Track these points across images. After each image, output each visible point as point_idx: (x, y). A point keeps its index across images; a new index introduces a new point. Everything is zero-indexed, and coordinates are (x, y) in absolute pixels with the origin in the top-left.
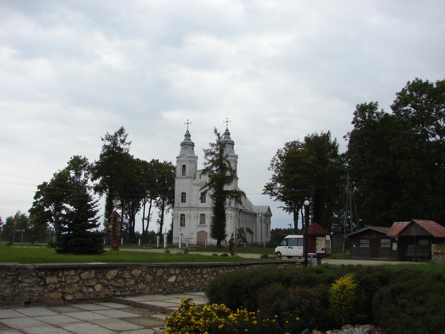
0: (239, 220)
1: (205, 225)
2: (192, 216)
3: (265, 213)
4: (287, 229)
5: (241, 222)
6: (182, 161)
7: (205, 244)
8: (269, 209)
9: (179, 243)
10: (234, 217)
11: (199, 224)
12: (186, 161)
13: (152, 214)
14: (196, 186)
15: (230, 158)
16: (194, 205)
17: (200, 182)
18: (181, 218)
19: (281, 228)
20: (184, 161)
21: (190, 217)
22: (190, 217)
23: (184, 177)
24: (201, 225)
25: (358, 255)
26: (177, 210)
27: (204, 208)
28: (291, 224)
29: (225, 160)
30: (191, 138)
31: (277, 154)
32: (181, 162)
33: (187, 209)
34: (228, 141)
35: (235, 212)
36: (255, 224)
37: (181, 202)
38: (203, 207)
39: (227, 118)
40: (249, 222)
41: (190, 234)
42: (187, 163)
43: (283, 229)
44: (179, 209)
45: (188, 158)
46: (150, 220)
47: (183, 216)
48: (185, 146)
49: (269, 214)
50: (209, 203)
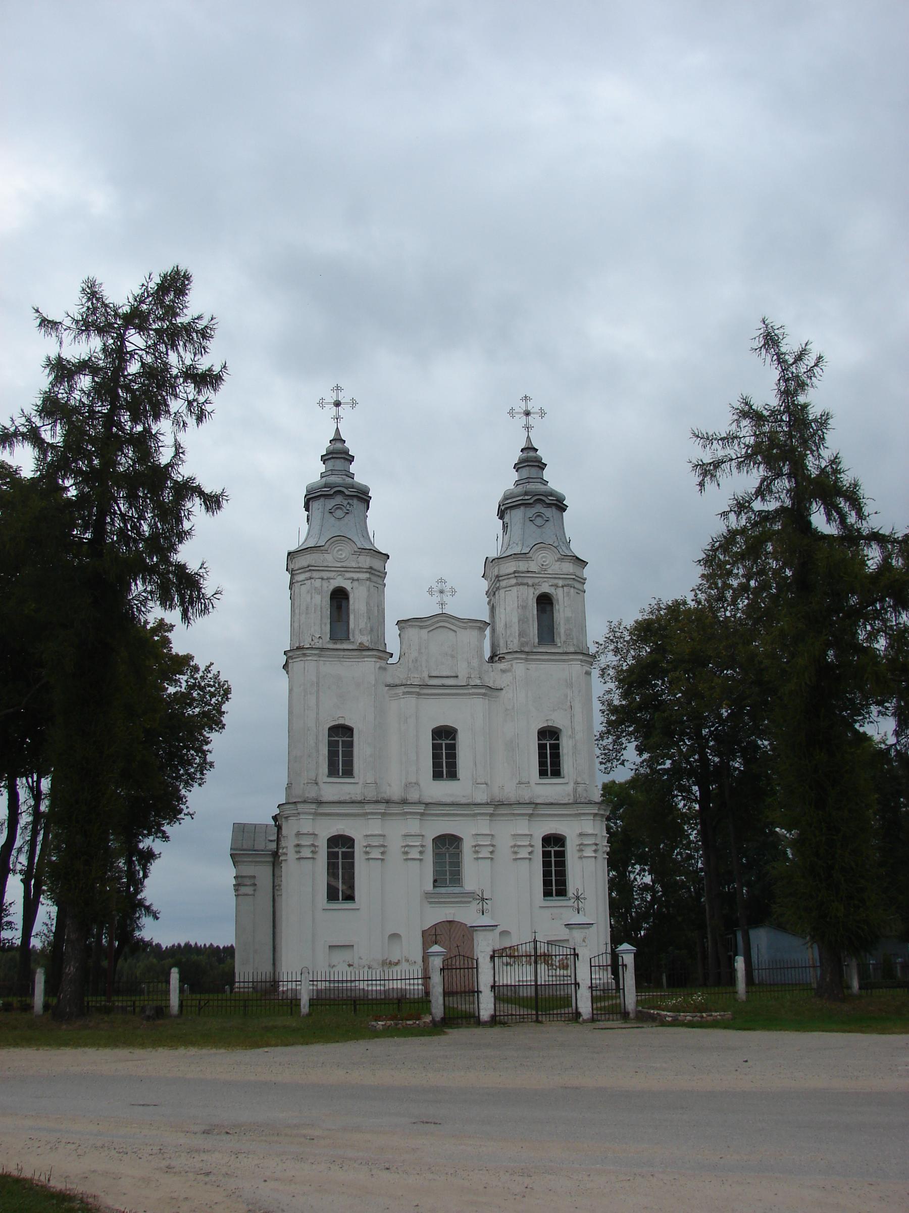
1: (457, 890)
2: (395, 845)
6: (327, 568)
9: (577, 984)
11: (429, 887)
12: (346, 569)
14: (404, 693)
17: (425, 675)
18: (546, 854)
20: (343, 570)
22: (406, 853)
23: (338, 646)
24: (438, 890)
26: (310, 814)
27: (453, 804)
30: (547, 474)
32: (325, 575)
33: (369, 808)
38: (448, 800)
39: (526, 398)
42: (353, 580)
44: (321, 810)
45: (361, 558)
48: (339, 500)
50: (479, 781)
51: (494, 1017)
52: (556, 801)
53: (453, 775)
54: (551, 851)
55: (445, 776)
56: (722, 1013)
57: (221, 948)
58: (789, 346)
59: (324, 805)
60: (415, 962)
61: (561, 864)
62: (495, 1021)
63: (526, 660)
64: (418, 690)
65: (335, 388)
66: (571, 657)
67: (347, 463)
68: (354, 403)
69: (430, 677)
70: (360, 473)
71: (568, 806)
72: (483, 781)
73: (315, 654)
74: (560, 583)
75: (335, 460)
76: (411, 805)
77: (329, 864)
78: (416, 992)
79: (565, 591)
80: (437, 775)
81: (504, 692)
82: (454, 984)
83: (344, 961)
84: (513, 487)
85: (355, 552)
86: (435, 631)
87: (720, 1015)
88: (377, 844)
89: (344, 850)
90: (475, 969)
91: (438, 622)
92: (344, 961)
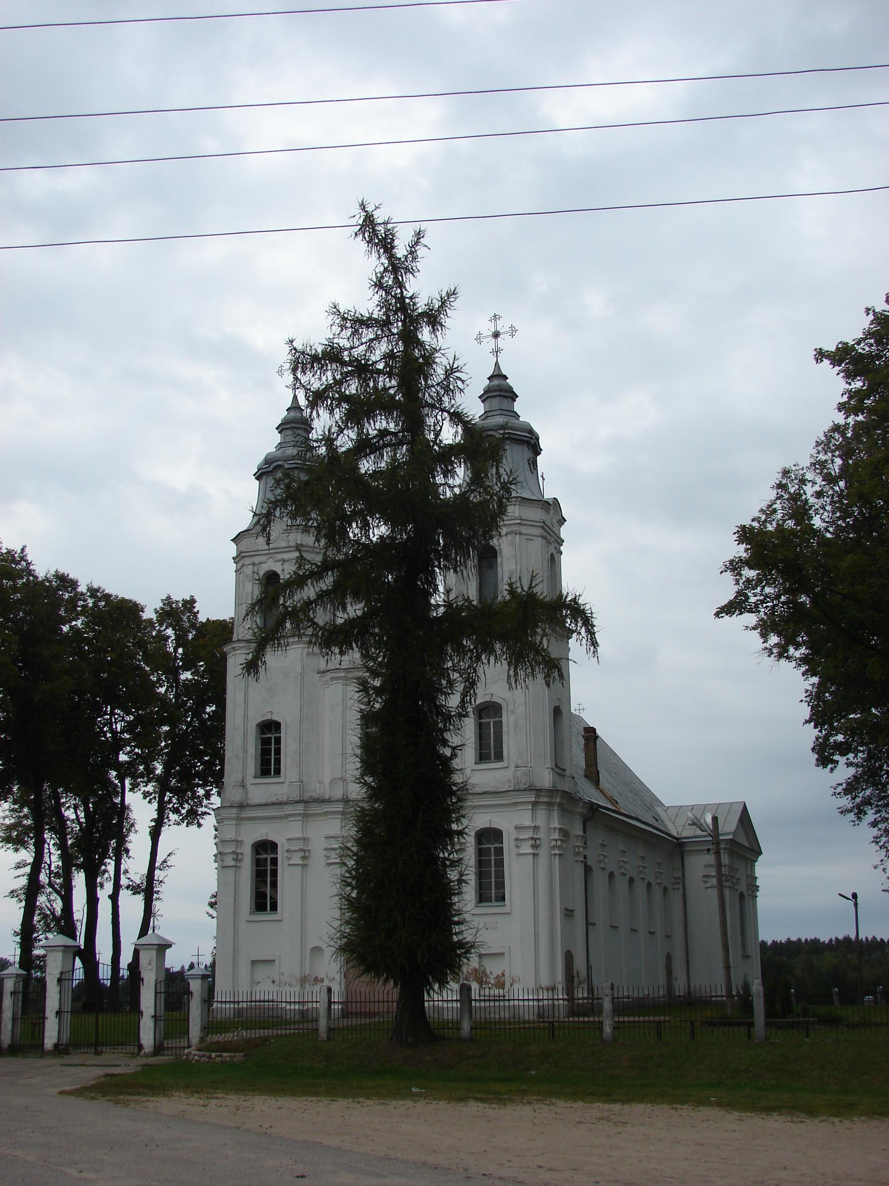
0: (588, 870)
3: (730, 837)
4: (783, 941)
5: (599, 880)
7: (317, 1020)
8: (745, 818)
10: (554, 847)
13: (165, 861)
14: (333, 679)
15: (517, 515)
16: (325, 790)
19: (765, 940)
21: (302, 854)
25: (578, 976)
26: (232, 819)
28: (855, 896)
29: (443, 410)
31: (779, 497)
32: (256, 560)
33: (288, 810)
34: (512, 429)
35: (555, 815)
36: (676, 898)
37: (255, 777)
40: (649, 885)
41: (308, 954)
42: (284, 561)
43: (769, 942)
46: (158, 892)
47: (266, 853)
49: (746, 844)
51: (56, 1045)
52: (494, 790)
54: (491, 848)
55: (272, 774)
56: (233, 1054)
57: (803, 941)
60: (334, 979)
62: (60, 1050)
65: (493, 318)
68: (479, 339)
71: (501, 795)
73: (243, 647)
75: (491, 399)
76: (335, 803)
79: (509, 540)
83: (268, 978)
84: (274, 450)
85: (284, 530)
87: (230, 1056)
88: (297, 849)
90: (158, 991)
92: (268, 978)
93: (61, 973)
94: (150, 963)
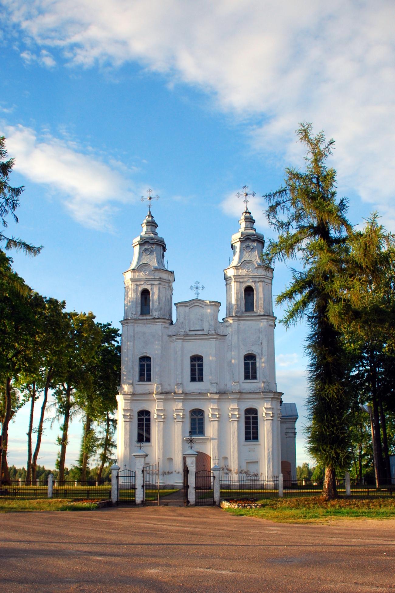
14: (176, 339)
17: (187, 330)
23: (145, 318)
37: (138, 381)
45: (156, 274)
50: (213, 382)
53: (201, 379)
58: (313, 135)
59: (243, 394)
61: (256, 423)
62: (144, 503)
63: (239, 320)
64: (182, 337)
66: (261, 318)
67: (154, 227)
69: (190, 331)
70: (161, 232)
72: (215, 382)
74: (257, 280)
77: (138, 424)
78: (127, 486)
80: (193, 379)
81: (227, 337)
82: (199, 483)
86: (193, 308)
89: (146, 417)
90: (134, 477)
91: (197, 303)
93: (144, 468)
94: (192, 463)
